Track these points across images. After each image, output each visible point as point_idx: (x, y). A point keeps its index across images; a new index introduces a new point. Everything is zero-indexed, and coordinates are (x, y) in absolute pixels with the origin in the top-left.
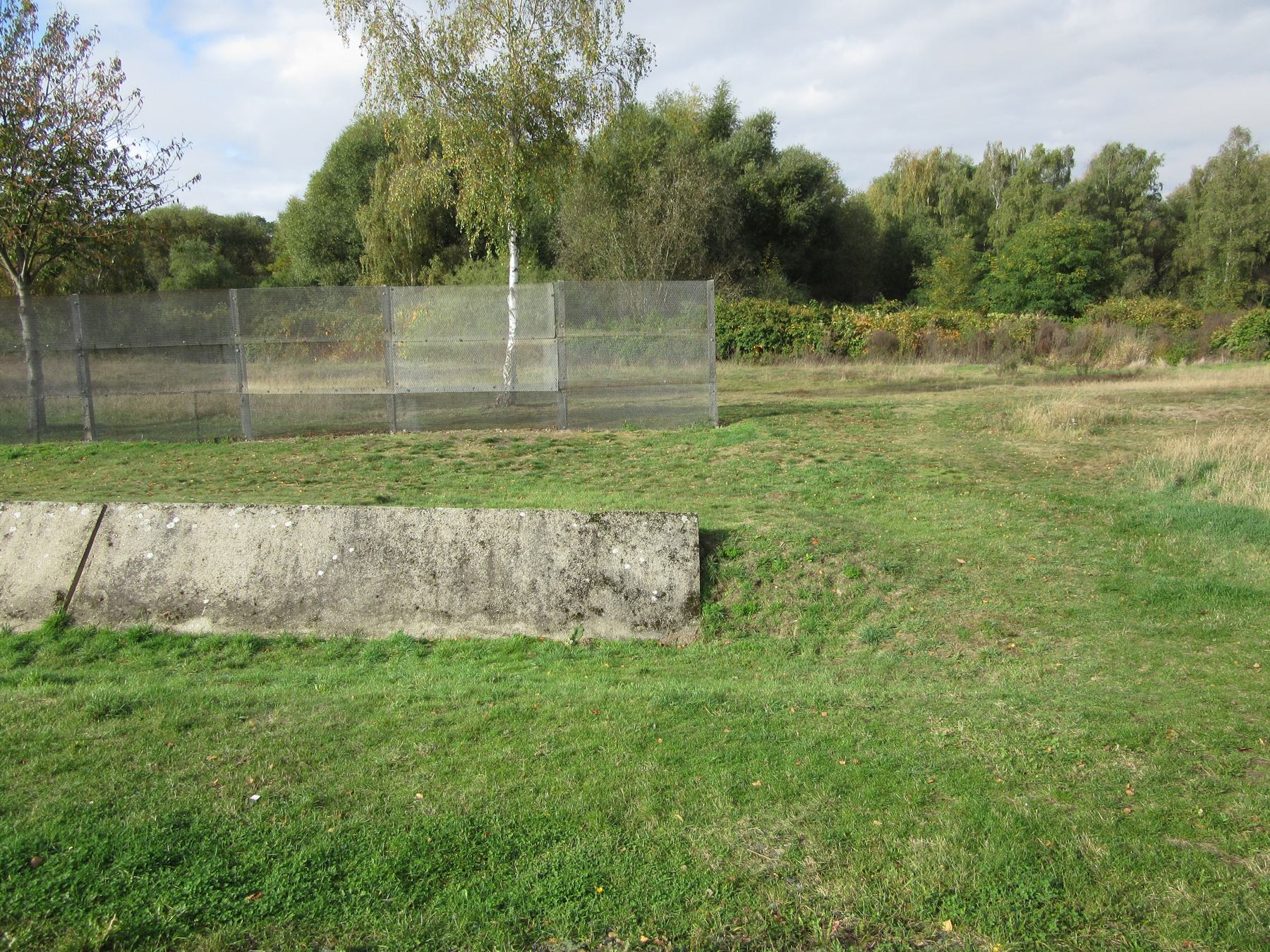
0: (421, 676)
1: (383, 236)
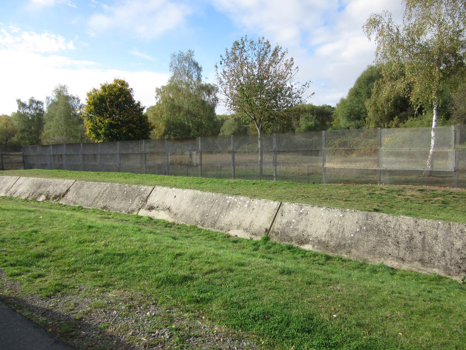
0: (394, 282)
1: (375, 110)
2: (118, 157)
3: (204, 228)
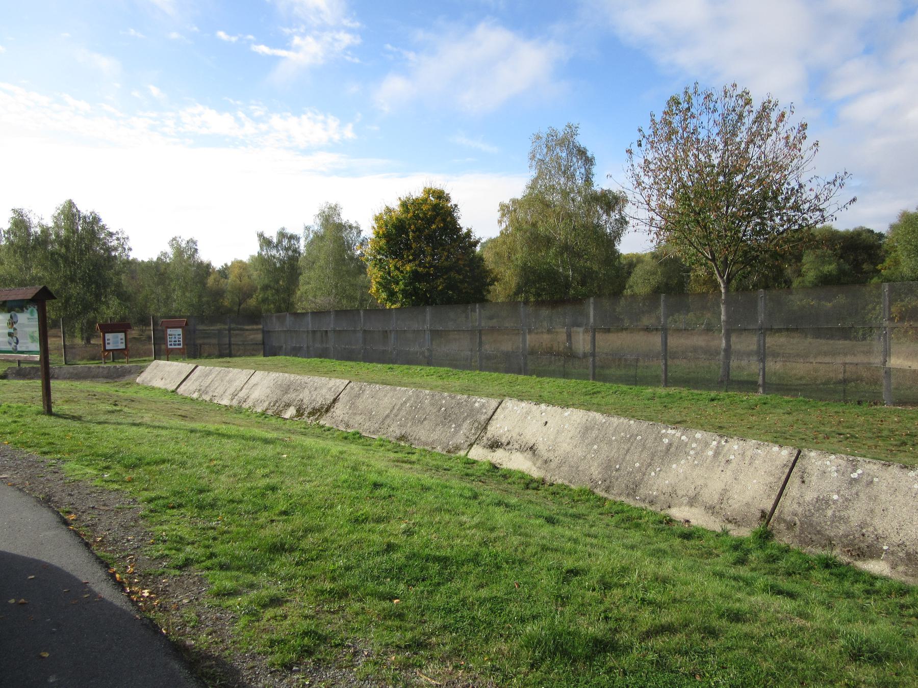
2: (428, 336)
3: (611, 497)
